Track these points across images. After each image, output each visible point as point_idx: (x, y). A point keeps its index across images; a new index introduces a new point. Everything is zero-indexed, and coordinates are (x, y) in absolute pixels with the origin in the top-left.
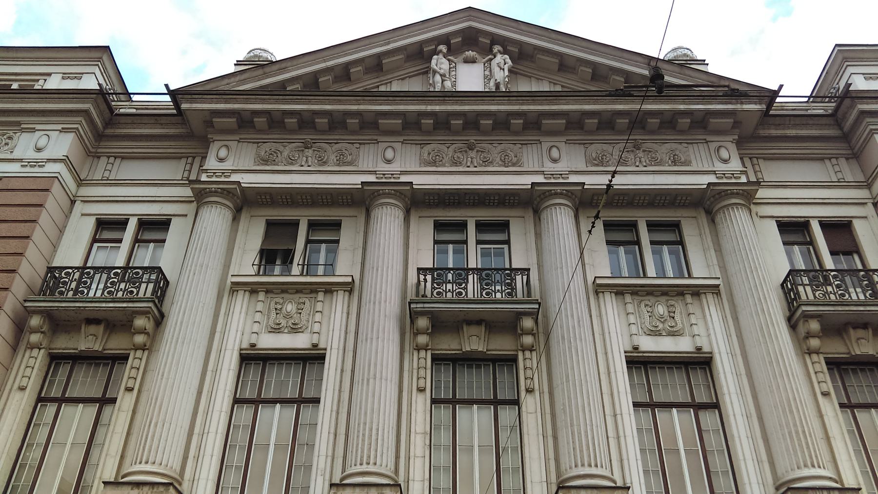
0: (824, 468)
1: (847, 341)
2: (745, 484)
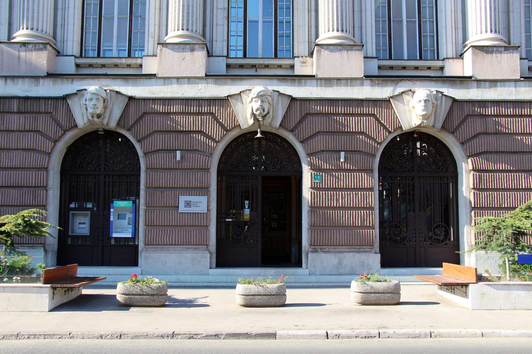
0: (499, 33)
2: (443, 44)
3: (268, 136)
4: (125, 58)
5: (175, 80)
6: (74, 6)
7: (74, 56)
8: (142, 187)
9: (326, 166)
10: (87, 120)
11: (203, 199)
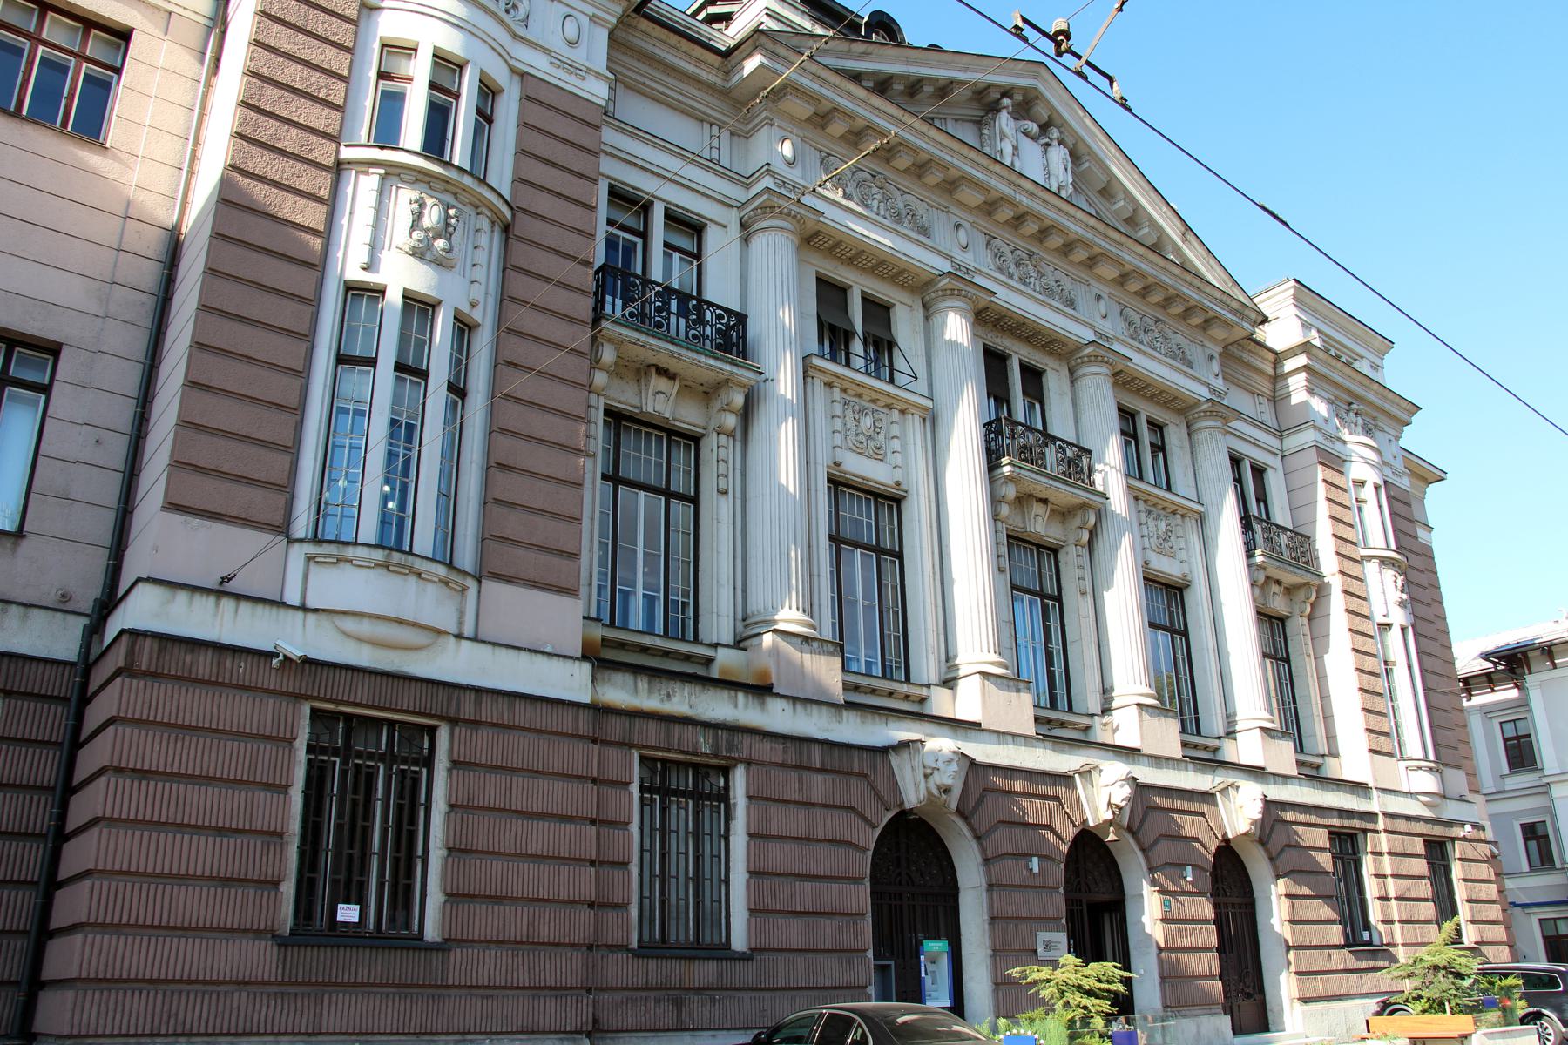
1: (643, 387)
5: (1010, 738)
9: (1172, 887)
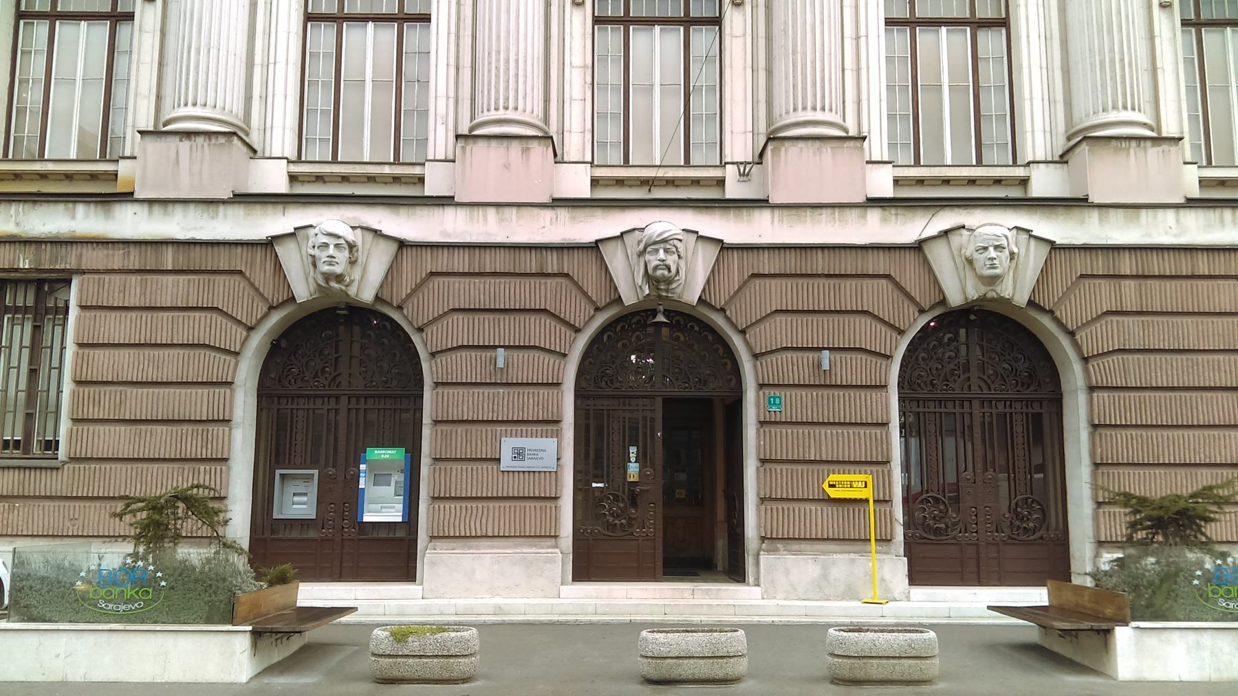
3: (675, 318)
4: (390, 164)
6: (287, 60)
7: (286, 158)
8: (426, 420)
10: (315, 286)
11: (550, 444)
